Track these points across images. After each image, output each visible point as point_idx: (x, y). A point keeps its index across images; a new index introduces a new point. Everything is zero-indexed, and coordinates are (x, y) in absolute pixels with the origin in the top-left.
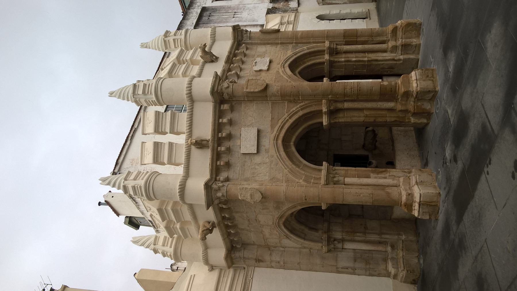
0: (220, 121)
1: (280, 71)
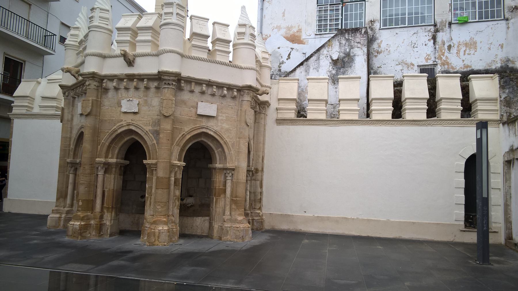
0: (183, 82)
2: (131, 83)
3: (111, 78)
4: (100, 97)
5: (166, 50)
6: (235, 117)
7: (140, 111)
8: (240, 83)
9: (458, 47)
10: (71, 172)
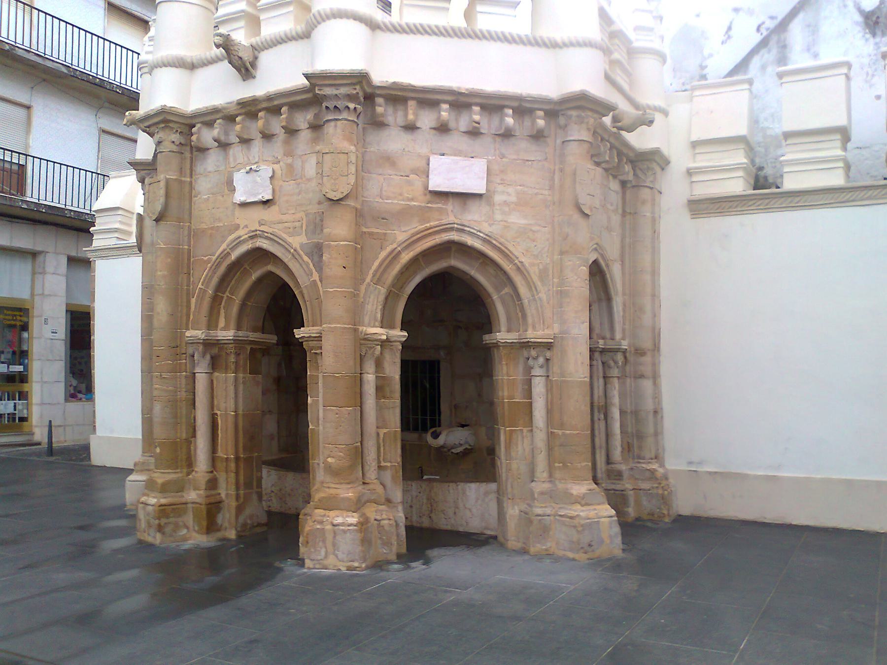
0: (380, 100)
1: (241, 232)
3: (208, 117)
4: (188, 171)
5: (322, 13)
6: (546, 192)
7: (277, 197)
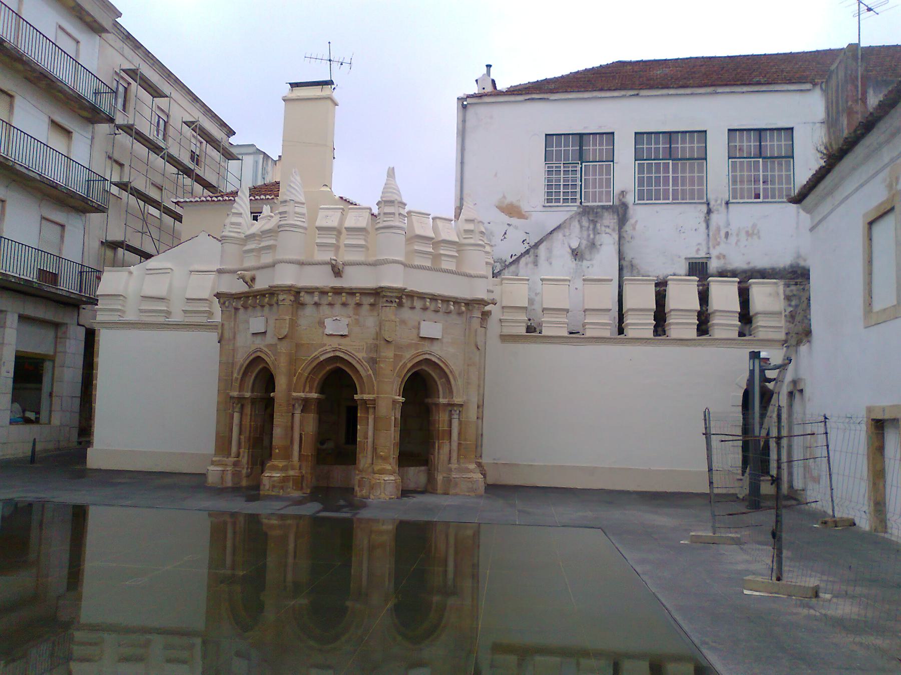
2: (336, 297)
3: (310, 291)
8: (467, 295)
9: (738, 235)
10: (237, 410)
